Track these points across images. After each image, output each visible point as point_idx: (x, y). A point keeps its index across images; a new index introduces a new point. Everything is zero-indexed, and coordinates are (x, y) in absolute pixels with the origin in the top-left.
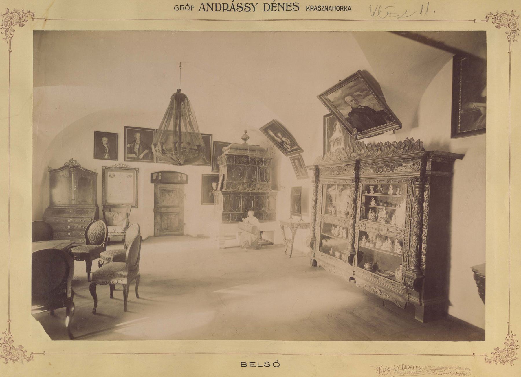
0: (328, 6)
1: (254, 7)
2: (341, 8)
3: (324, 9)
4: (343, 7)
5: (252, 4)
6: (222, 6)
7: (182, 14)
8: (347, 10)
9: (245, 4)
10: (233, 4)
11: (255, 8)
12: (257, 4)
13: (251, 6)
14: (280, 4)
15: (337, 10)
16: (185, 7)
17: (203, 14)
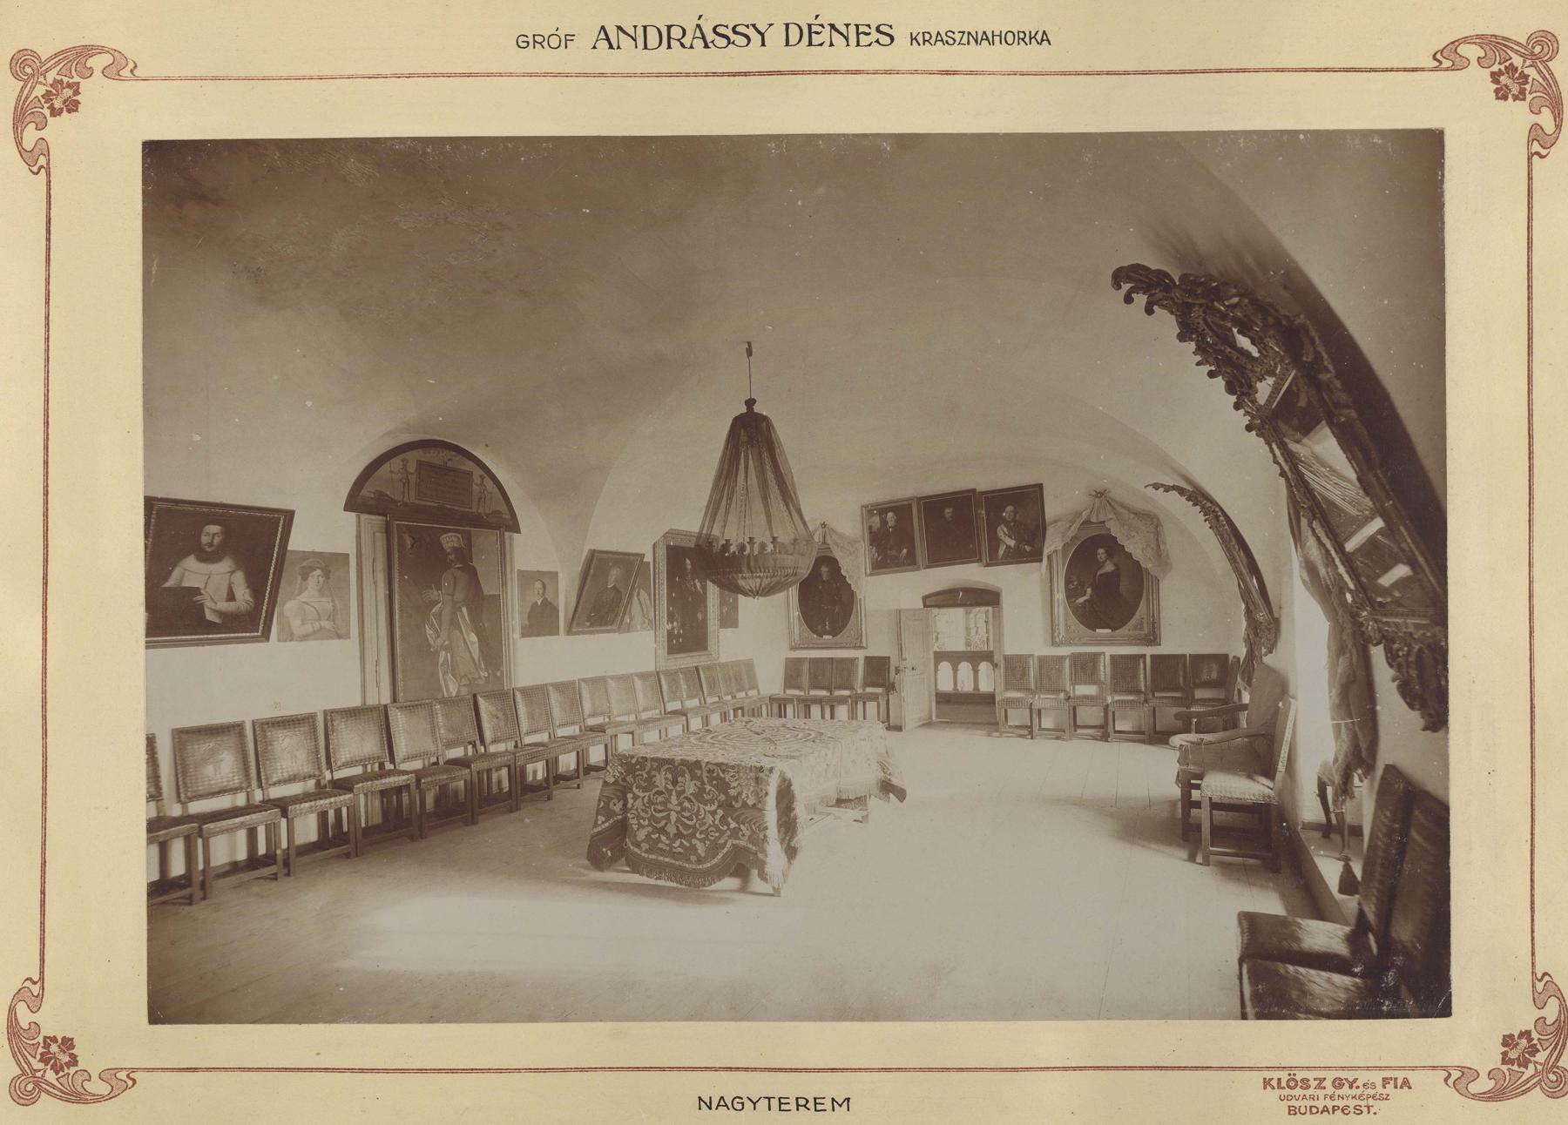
1: (762, 35)
2: (669, 38)
3: (965, 40)
4: (1024, 32)
6: (803, 28)
8: (1039, 41)
9: (717, 26)
10: (698, 26)
11: (765, 34)
12: (771, 25)
13: (751, 32)
15: (1006, 42)
16: (546, 40)
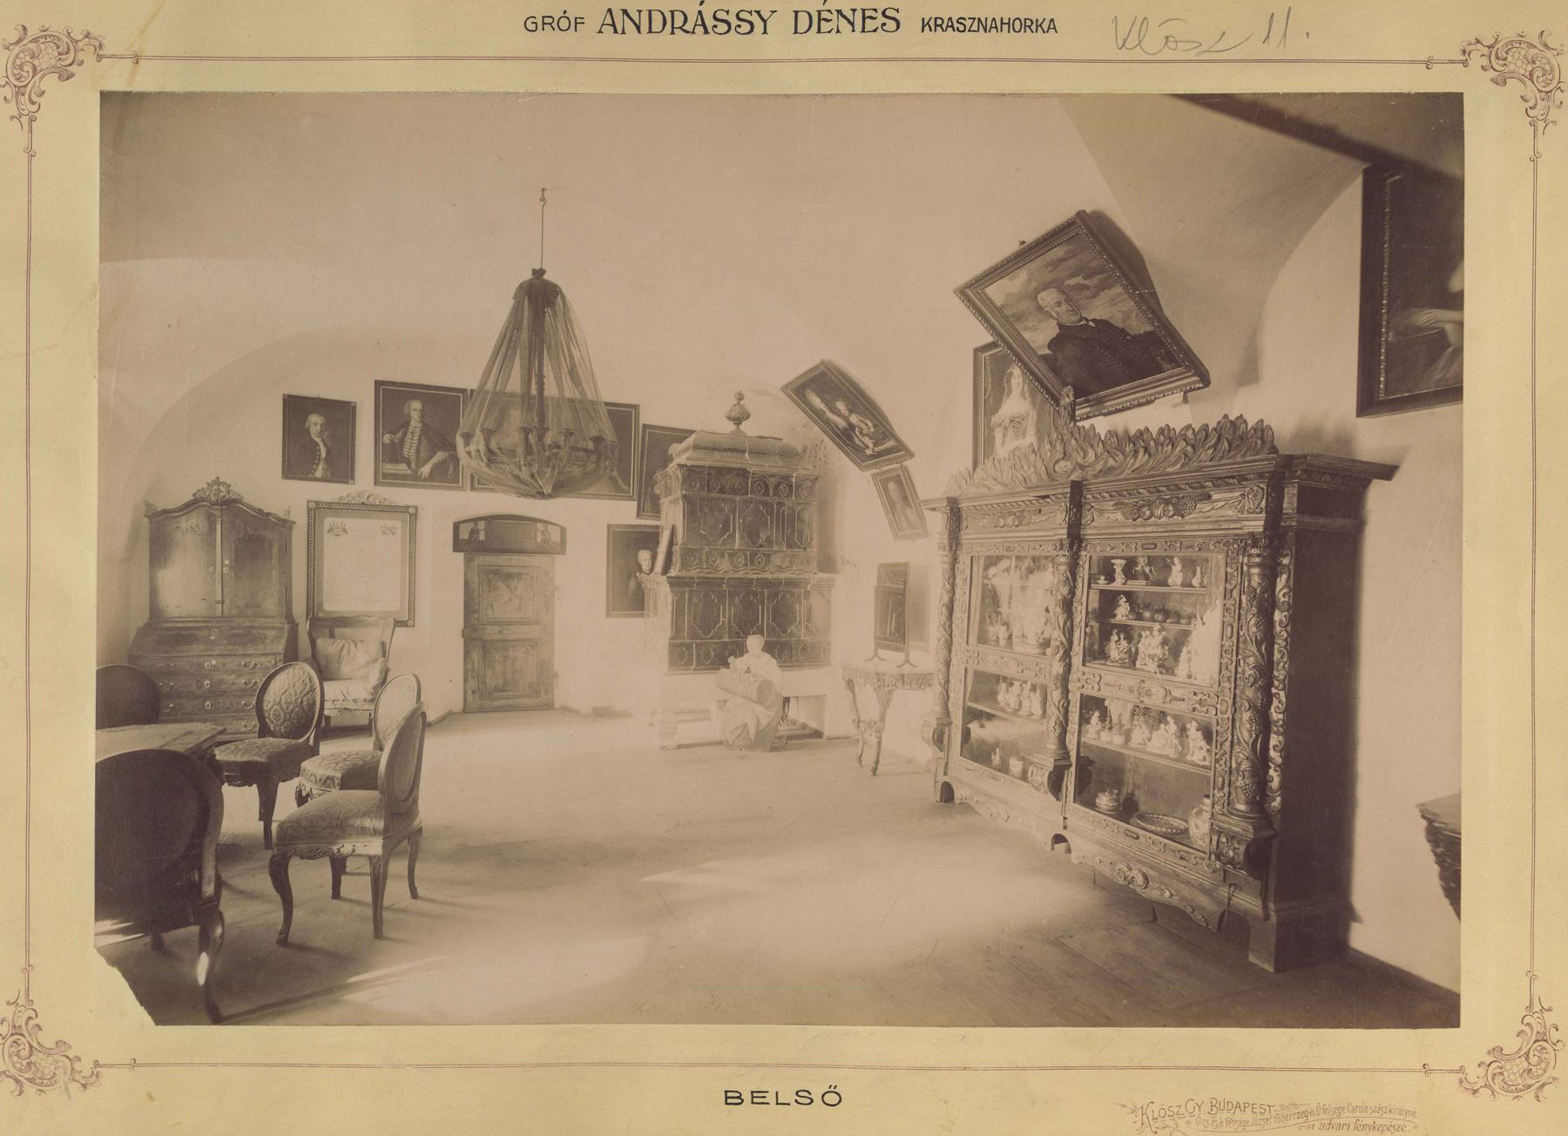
0: (986, 19)
1: (765, 21)
2: (1025, 25)
3: (975, 27)
4: (1031, 21)
5: (758, 12)
6: (667, 19)
7: (547, 41)
8: (1046, 30)
9: (739, 13)
10: (700, 12)
11: (768, 23)
12: (773, 12)
13: (755, 19)
14: (844, 13)
15: (1014, 30)
17: (610, 43)
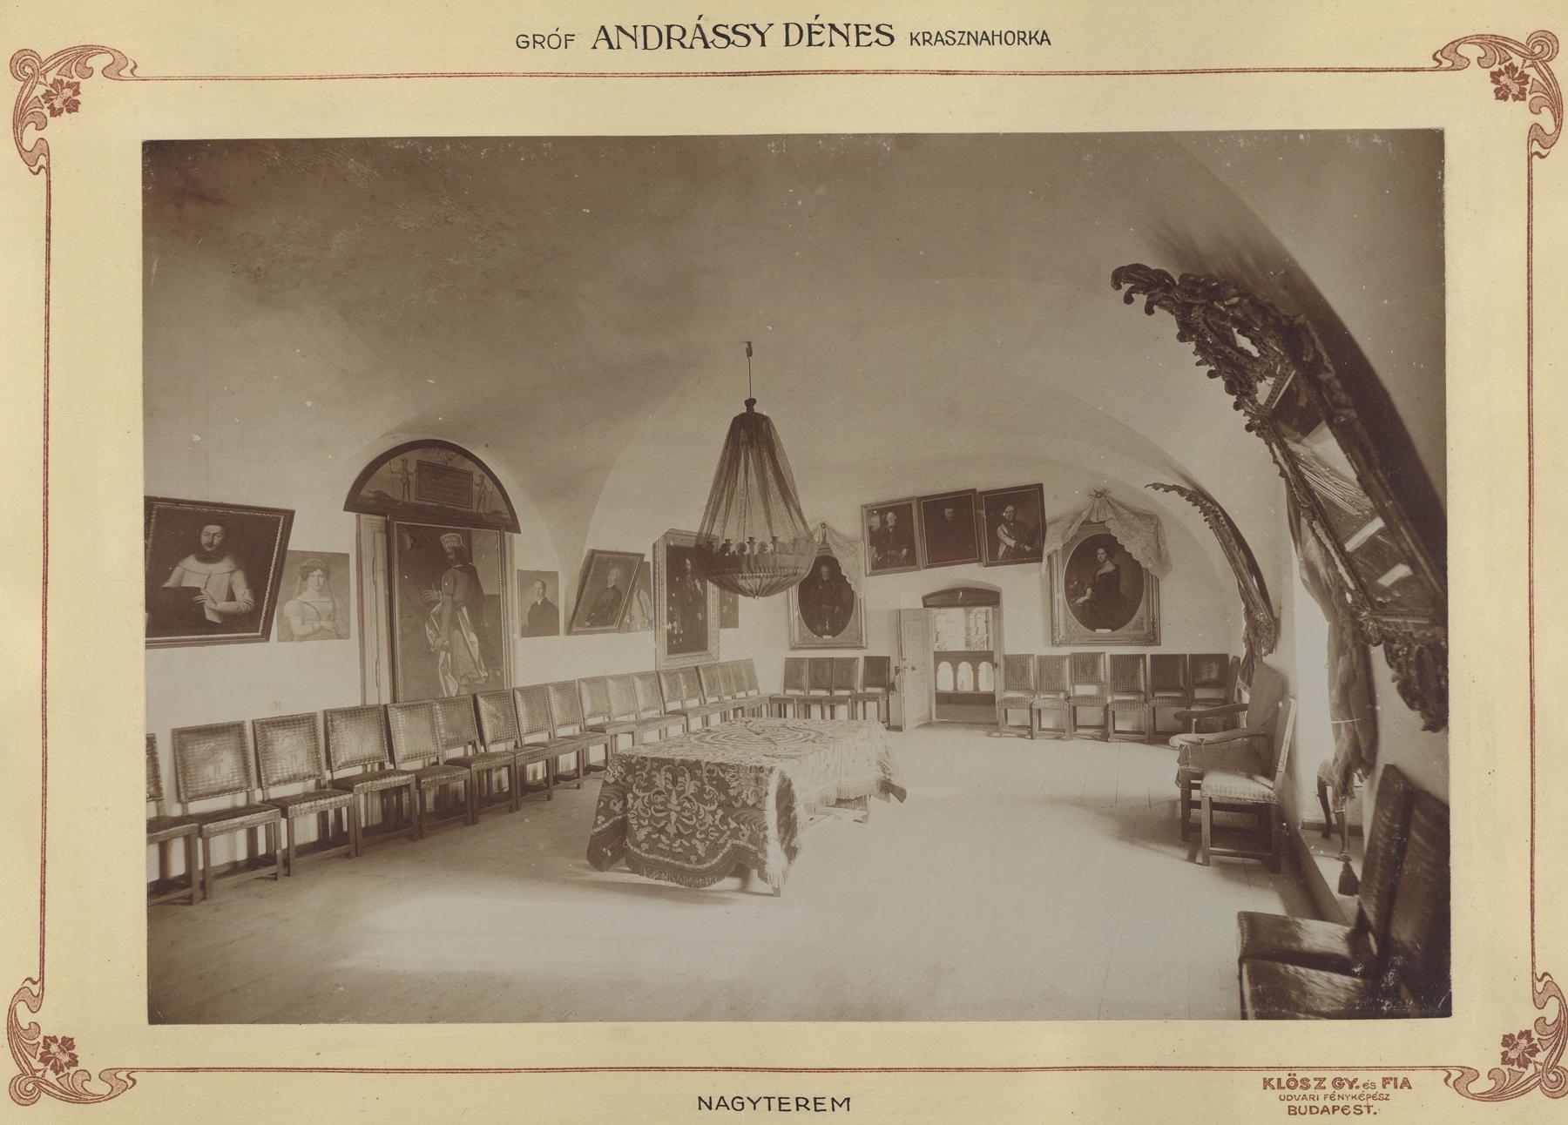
1: (762, 35)
2: (669, 38)
3: (965, 40)
4: (1024, 32)
6: (803, 28)
8: (1039, 41)
9: (717, 26)
10: (698, 26)
11: (765, 34)
12: (771, 25)
13: (751, 32)
15: (1006, 42)
